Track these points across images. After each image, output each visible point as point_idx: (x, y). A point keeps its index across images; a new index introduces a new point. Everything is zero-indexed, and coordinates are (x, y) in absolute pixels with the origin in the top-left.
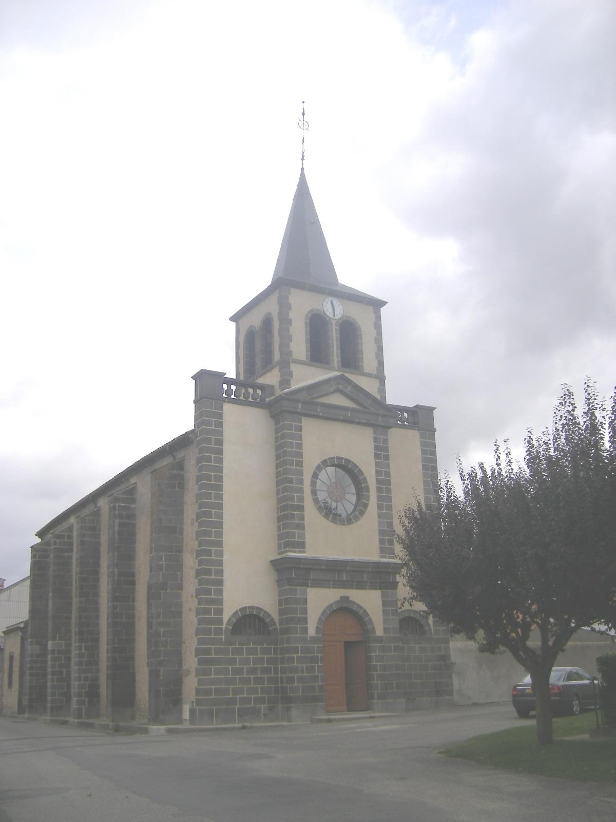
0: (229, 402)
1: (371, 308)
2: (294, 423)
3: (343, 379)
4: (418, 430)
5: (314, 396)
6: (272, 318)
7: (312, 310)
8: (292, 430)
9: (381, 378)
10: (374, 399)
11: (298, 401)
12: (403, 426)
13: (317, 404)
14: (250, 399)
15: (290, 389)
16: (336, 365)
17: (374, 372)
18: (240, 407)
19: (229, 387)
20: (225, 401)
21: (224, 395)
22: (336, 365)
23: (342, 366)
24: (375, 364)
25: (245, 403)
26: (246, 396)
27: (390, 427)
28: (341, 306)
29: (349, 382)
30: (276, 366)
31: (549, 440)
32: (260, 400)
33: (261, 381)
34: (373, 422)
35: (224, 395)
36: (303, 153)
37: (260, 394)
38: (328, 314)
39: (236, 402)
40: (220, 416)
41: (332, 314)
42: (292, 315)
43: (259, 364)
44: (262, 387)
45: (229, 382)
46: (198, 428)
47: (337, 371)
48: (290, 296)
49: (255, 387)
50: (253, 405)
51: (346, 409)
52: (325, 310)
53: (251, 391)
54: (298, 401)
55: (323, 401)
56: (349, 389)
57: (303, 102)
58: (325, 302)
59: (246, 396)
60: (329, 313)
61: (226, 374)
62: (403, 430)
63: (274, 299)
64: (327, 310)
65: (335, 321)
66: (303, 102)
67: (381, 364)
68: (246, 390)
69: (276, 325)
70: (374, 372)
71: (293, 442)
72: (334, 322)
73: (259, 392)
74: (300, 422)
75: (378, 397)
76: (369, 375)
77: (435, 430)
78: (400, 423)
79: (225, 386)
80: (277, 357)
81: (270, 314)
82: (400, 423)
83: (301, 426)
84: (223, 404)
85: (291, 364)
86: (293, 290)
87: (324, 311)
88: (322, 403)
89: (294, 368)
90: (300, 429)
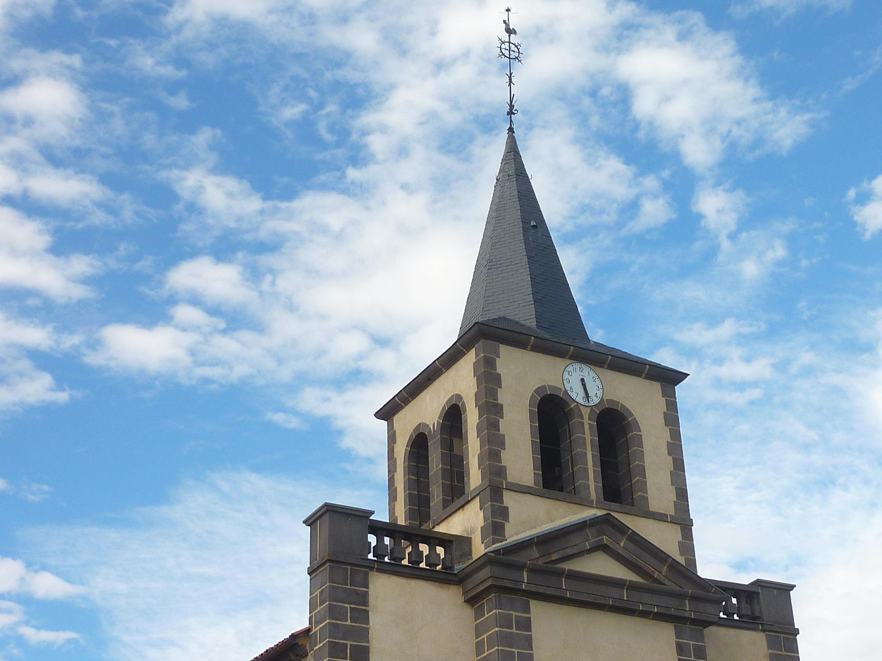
0: (380, 570)
1: (656, 386)
2: (514, 613)
3: (606, 522)
4: (764, 631)
5: (554, 557)
6: (464, 404)
7: (543, 388)
8: (512, 628)
9: (686, 526)
10: (674, 565)
11: (521, 567)
12: (729, 623)
13: (560, 573)
14: (423, 565)
15: (504, 543)
16: (593, 495)
17: (670, 511)
18: (402, 581)
19: (380, 540)
20: (371, 568)
21: (371, 556)
22: (593, 495)
23: (606, 499)
24: (671, 495)
25: (413, 572)
26: (416, 558)
27: (707, 624)
28: (598, 382)
29: (622, 529)
30: (474, 497)
31: (326, 598)
32: (442, 568)
33: (441, 529)
34: (673, 611)
35: (371, 556)
36: (511, 102)
37: (442, 556)
38: (574, 396)
39: (395, 569)
40: (364, 599)
41: (582, 394)
42: (504, 397)
43: (436, 494)
44: (446, 541)
45: (378, 529)
46: (317, 624)
47: (597, 508)
48: (498, 360)
49: (434, 540)
50: (430, 576)
51: (619, 584)
52: (568, 388)
53: (424, 548)
54: (521, 567)
55: (560, 566)
56: (622, 545)
57: (508, 10)
58: (566, 373)
59: (416, 558)
60: (578, 395)
61: (372, 513)
62: (731, 632)
63: (467, 364)
64: (571, 388)
65: (589, 410)
66: (508, 10)
67: (682, 494)
68: (416, 548)
69: (472, 418)
70: (670, 511)
71: (512, 653)
72: (586, 412)
73: (440, 550)
74: (527, 610)
75: (681, 560)
76: (660, 517)
77: (797, 632)
78: (725, 617)
79: (372, 539)
80: (475, 478)
81: (459, 397)
82: (725, 617)
83: (529, 619)
84: (368, 575)
85: (505, 493)
86: (504, 349)
87: (566, 391)
88: (569, 571)
89: (510, 499)
90: (527, 625)
